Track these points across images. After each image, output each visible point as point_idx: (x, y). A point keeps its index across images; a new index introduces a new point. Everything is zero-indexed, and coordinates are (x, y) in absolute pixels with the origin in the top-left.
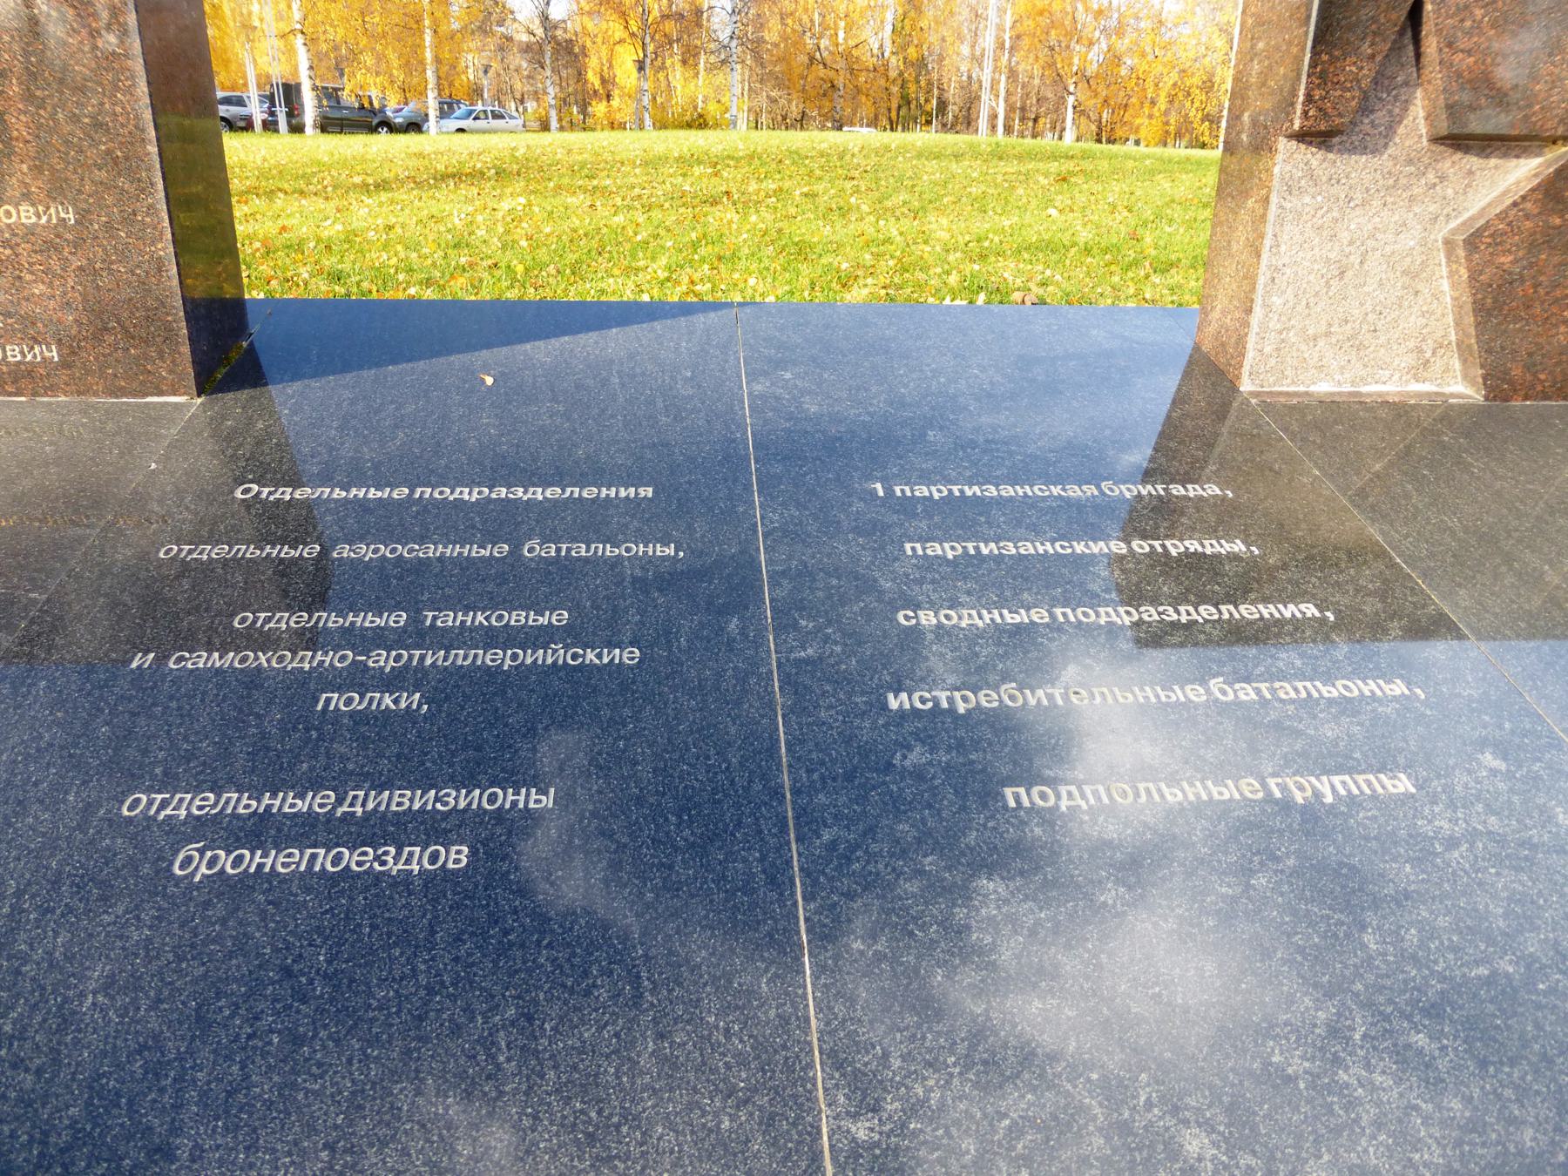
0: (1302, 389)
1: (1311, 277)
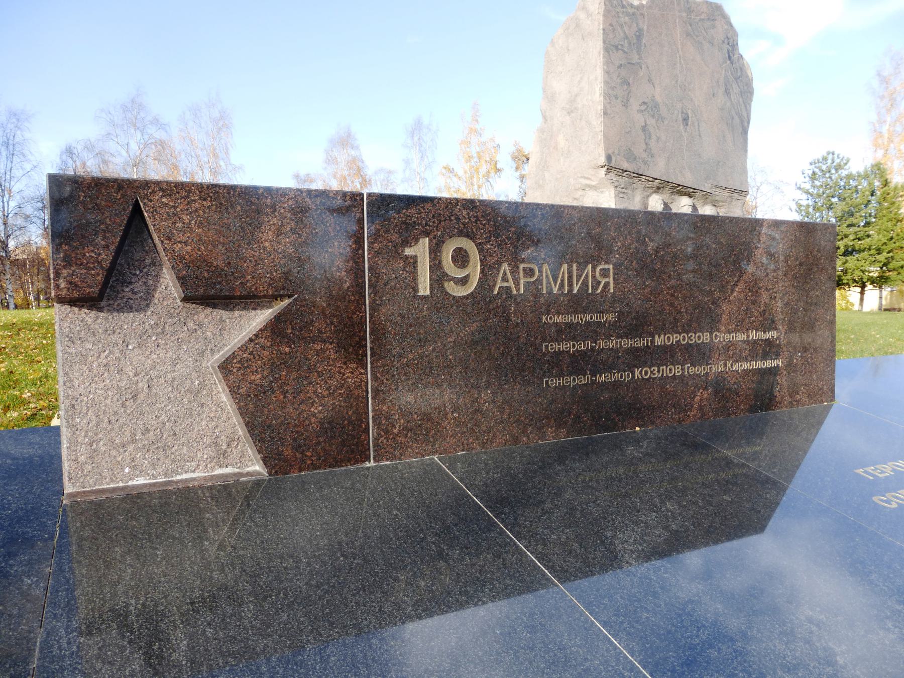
0: (121, 484)
1: (108, 401)
